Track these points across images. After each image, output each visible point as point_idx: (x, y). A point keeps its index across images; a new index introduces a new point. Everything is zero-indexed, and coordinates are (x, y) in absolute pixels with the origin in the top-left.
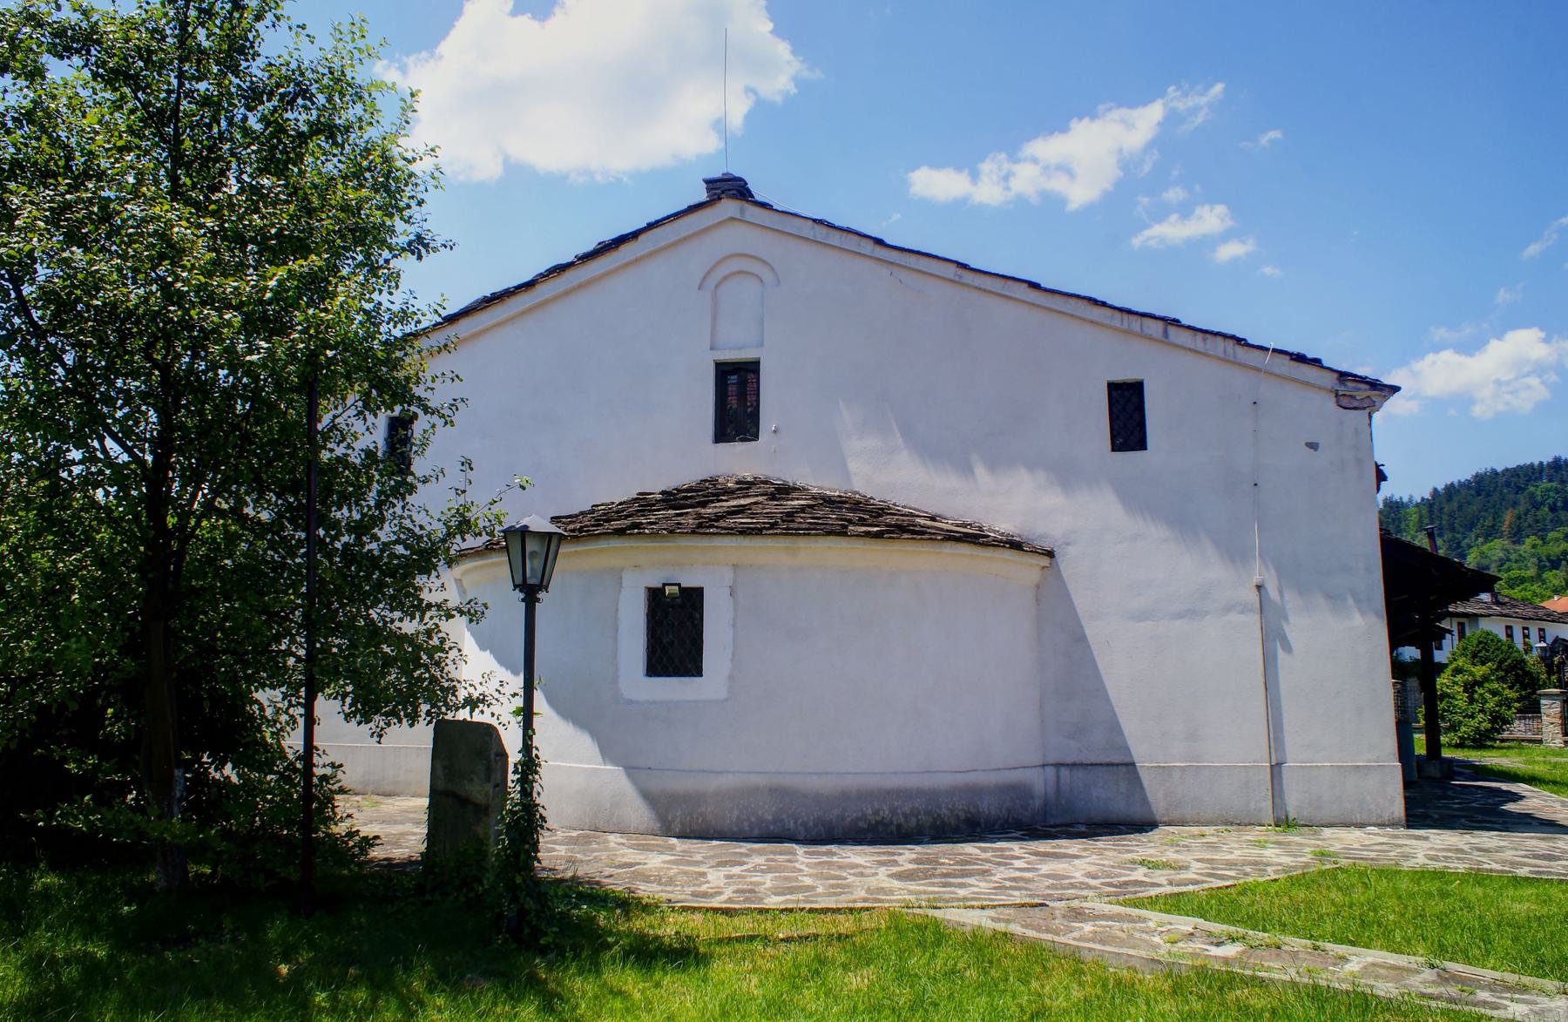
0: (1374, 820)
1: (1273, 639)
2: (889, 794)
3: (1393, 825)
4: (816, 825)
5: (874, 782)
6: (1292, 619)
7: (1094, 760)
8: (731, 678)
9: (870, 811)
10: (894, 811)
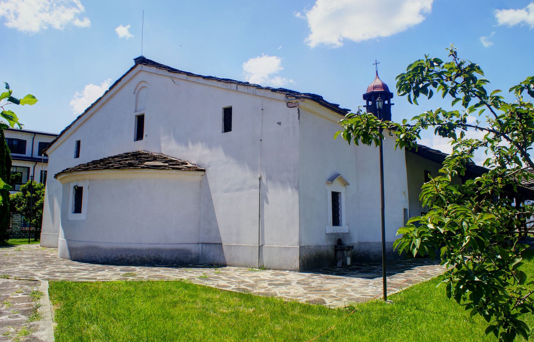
0: (289, 268)
1: (262, 198)
2: (125, 250)
3: (295, 270)
6: (269, 190)
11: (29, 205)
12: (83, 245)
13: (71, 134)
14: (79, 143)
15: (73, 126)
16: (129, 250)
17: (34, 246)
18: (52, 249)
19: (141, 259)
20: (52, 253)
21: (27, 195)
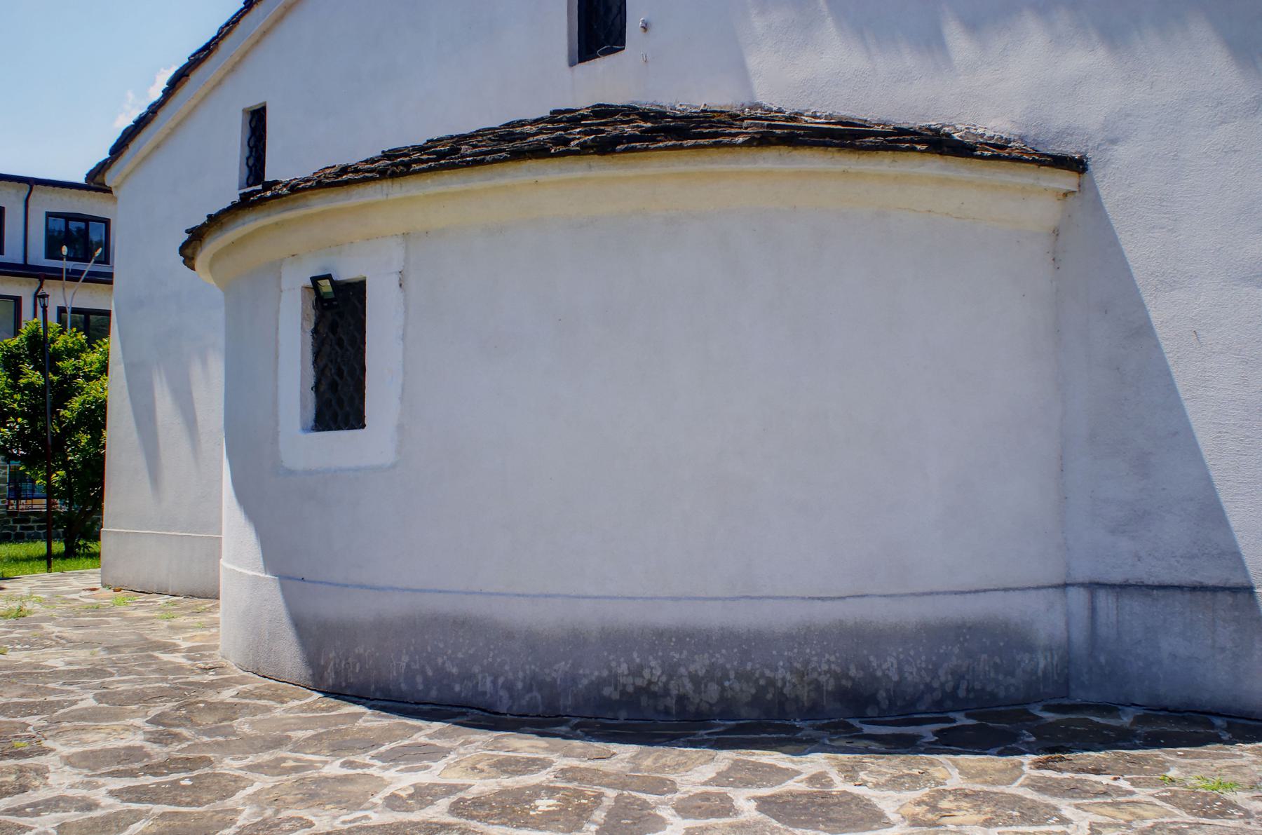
2: (662, 638)
4: (528, 688)
5: (631, 615)
7: (1167, 579)
8: (400, 428)
9: (624, 668)
10: (671, 671)
11: (33, 414)
12: (394, 607)
13: (220, 83)
14: (257, 120)
15: (225, 45)
16: (684, 638)
17: (78, 582)
18: (162, 600)
19: (762, 690)
20: (185, 635)
21: (23, 381)
